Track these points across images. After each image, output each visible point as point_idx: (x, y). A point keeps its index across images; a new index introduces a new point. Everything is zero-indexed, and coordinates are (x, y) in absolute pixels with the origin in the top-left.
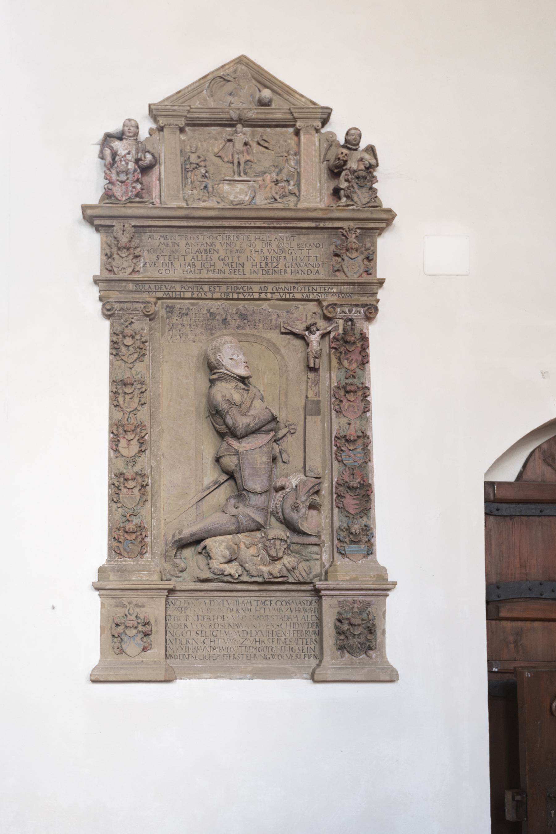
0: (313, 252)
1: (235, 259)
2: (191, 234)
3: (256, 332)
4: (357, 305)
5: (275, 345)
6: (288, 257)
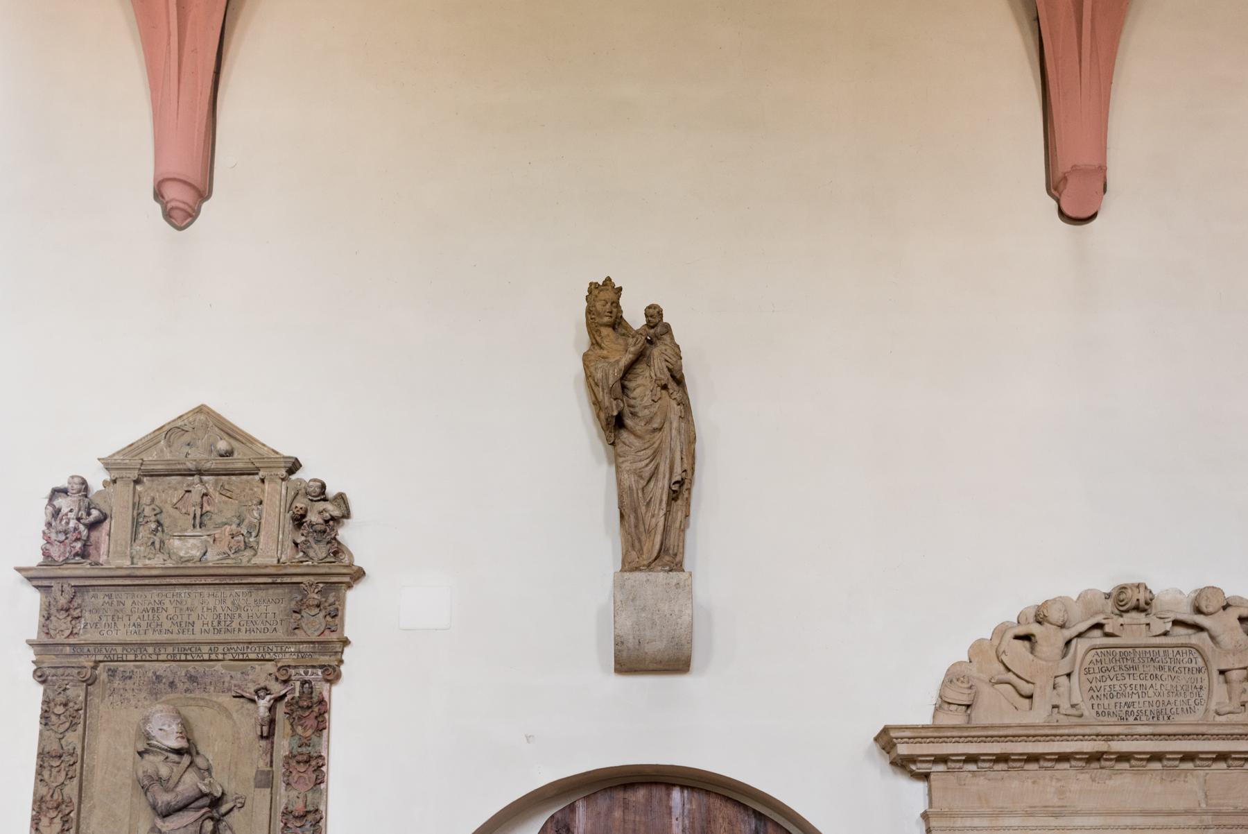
0: (272, 608)
1: (185, 618)
2: (138, 592)
3: (205, 696)
4: (313, 667)
5: (226, 710)
6: (244, 614)
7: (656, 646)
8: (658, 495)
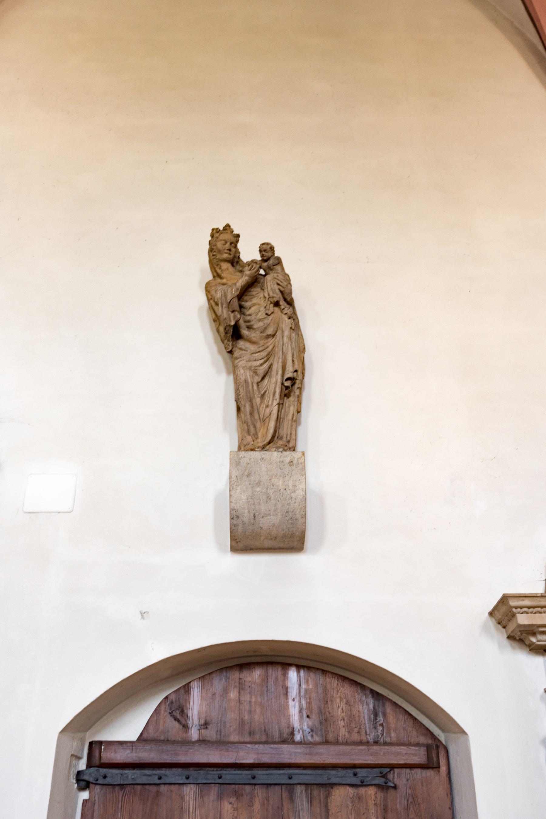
7: (271, 521)
8: (272, 389)
